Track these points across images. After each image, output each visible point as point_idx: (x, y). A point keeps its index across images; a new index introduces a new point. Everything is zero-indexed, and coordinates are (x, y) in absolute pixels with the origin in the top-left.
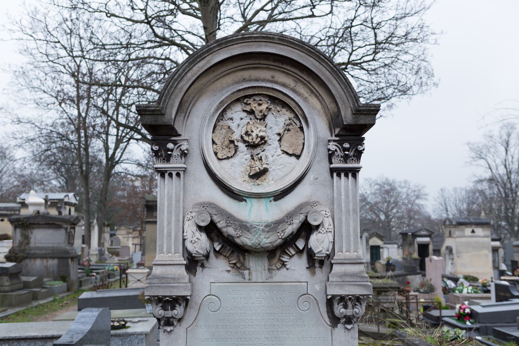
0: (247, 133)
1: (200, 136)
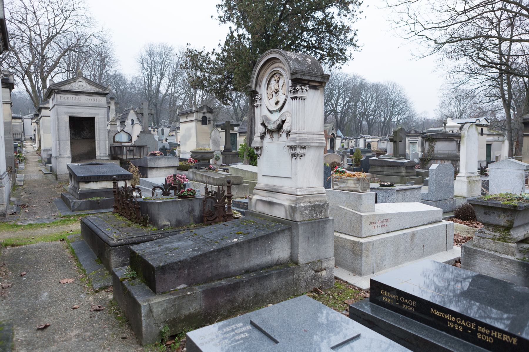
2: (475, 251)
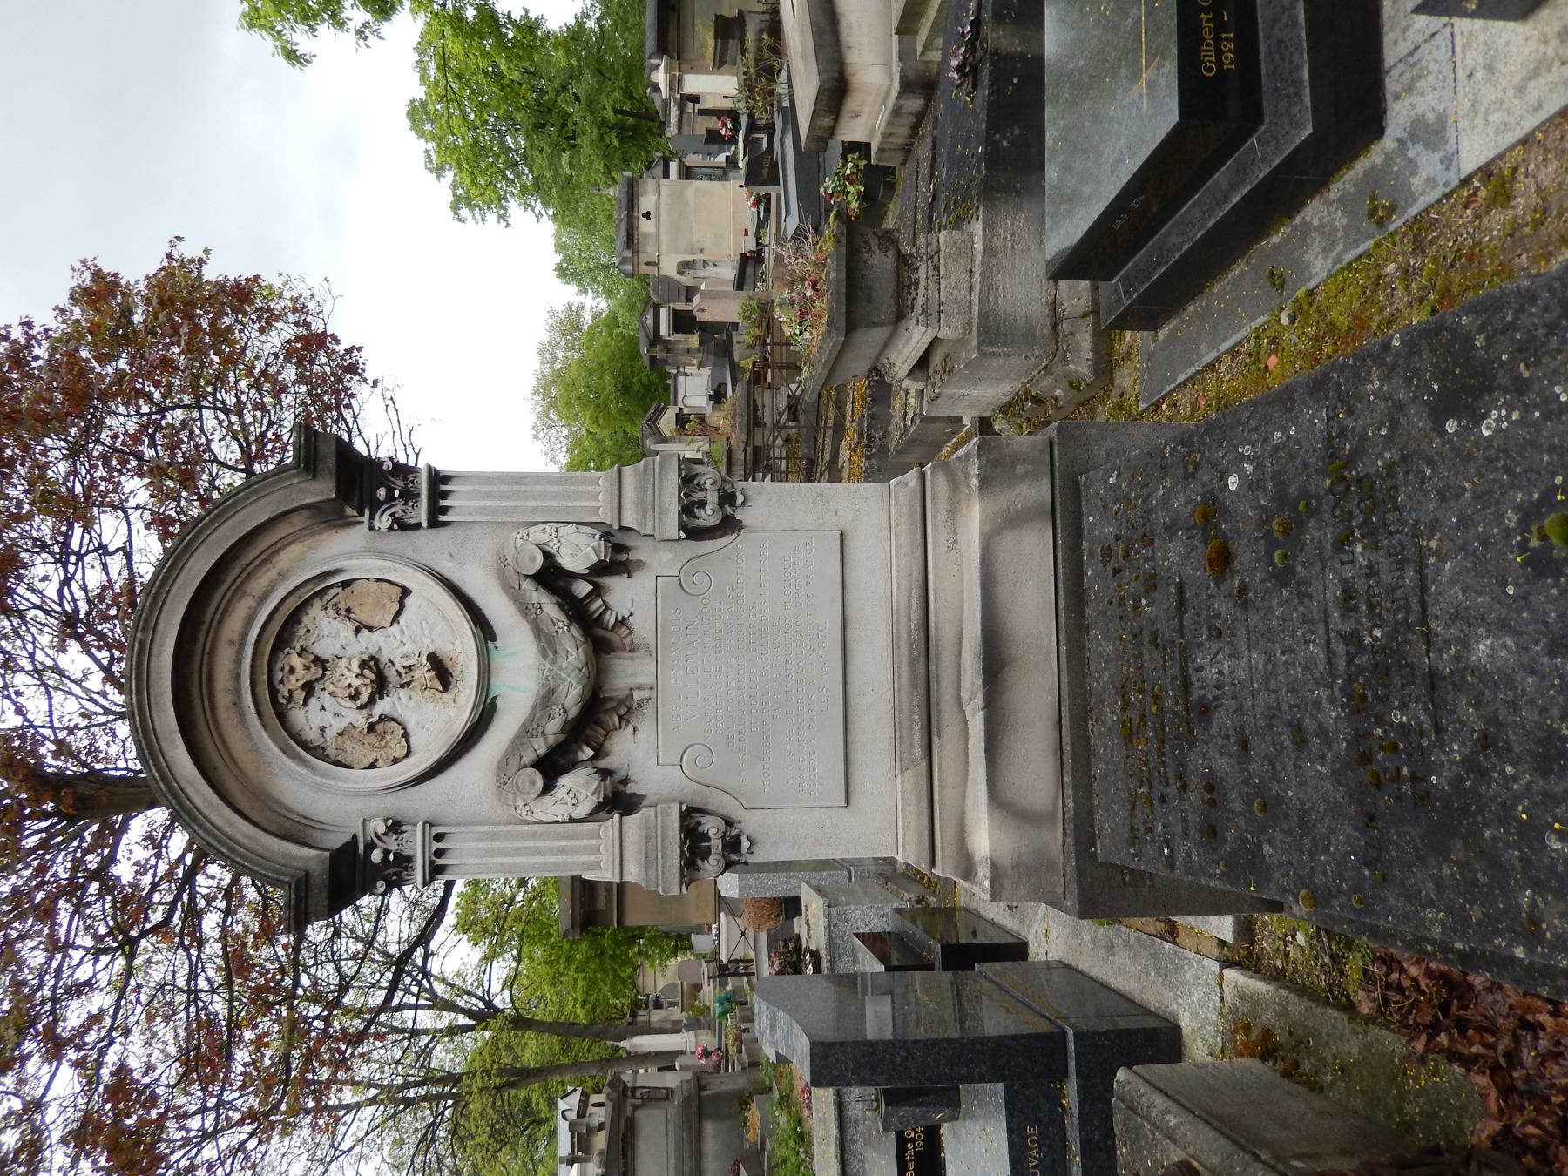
0: (354, 697)
1: (357, 795)
2: (984, 316)
